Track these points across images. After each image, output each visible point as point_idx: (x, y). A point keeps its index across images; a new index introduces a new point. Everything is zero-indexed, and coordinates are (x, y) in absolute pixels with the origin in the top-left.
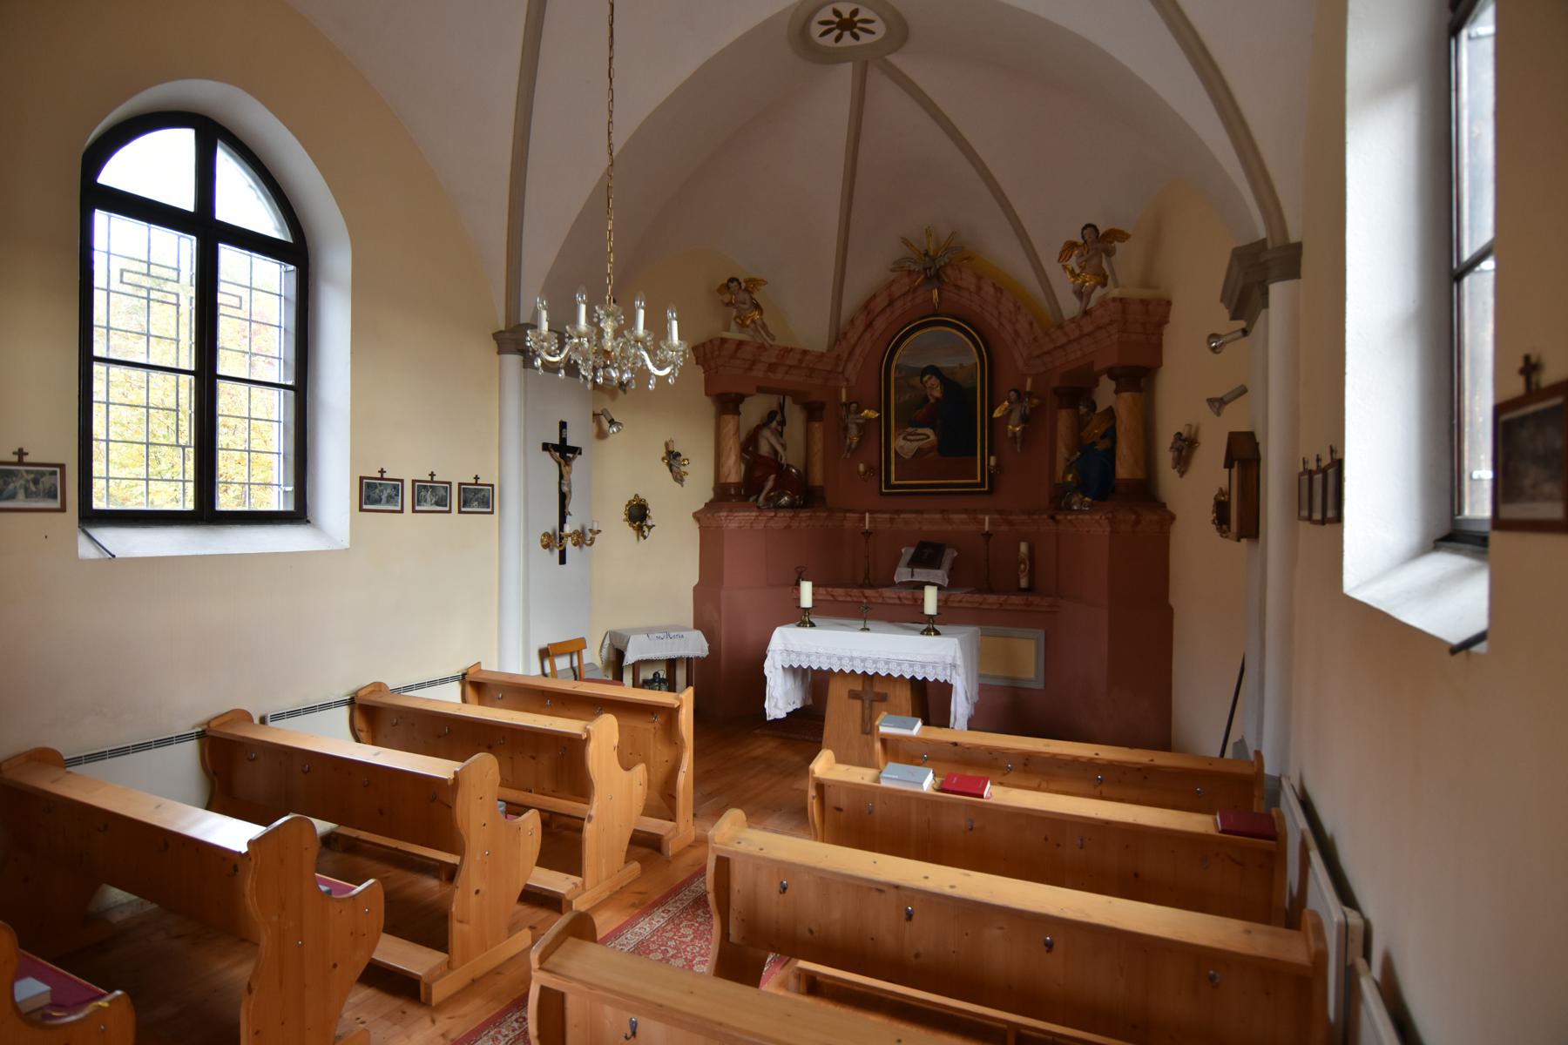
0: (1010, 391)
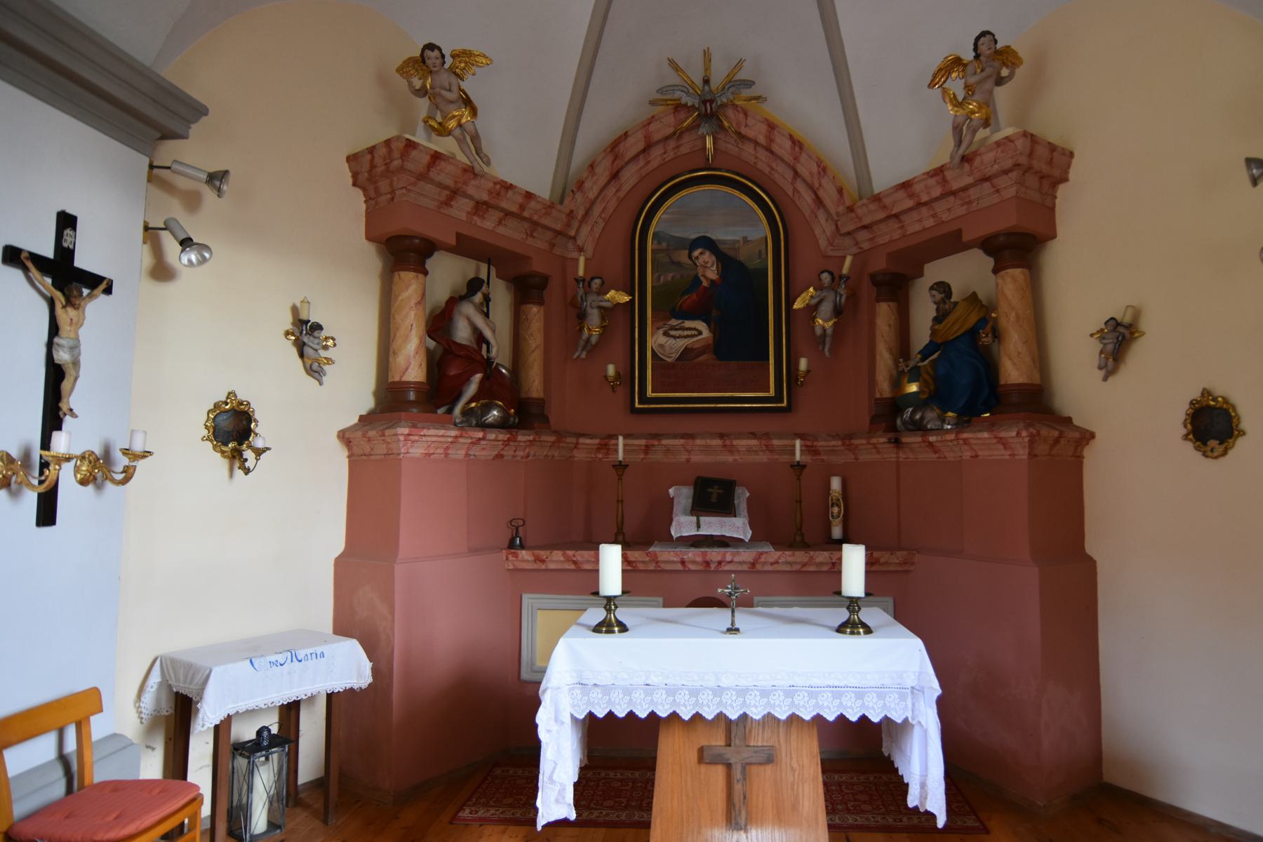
0: (822, 272)
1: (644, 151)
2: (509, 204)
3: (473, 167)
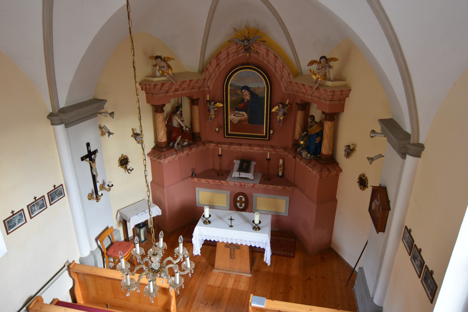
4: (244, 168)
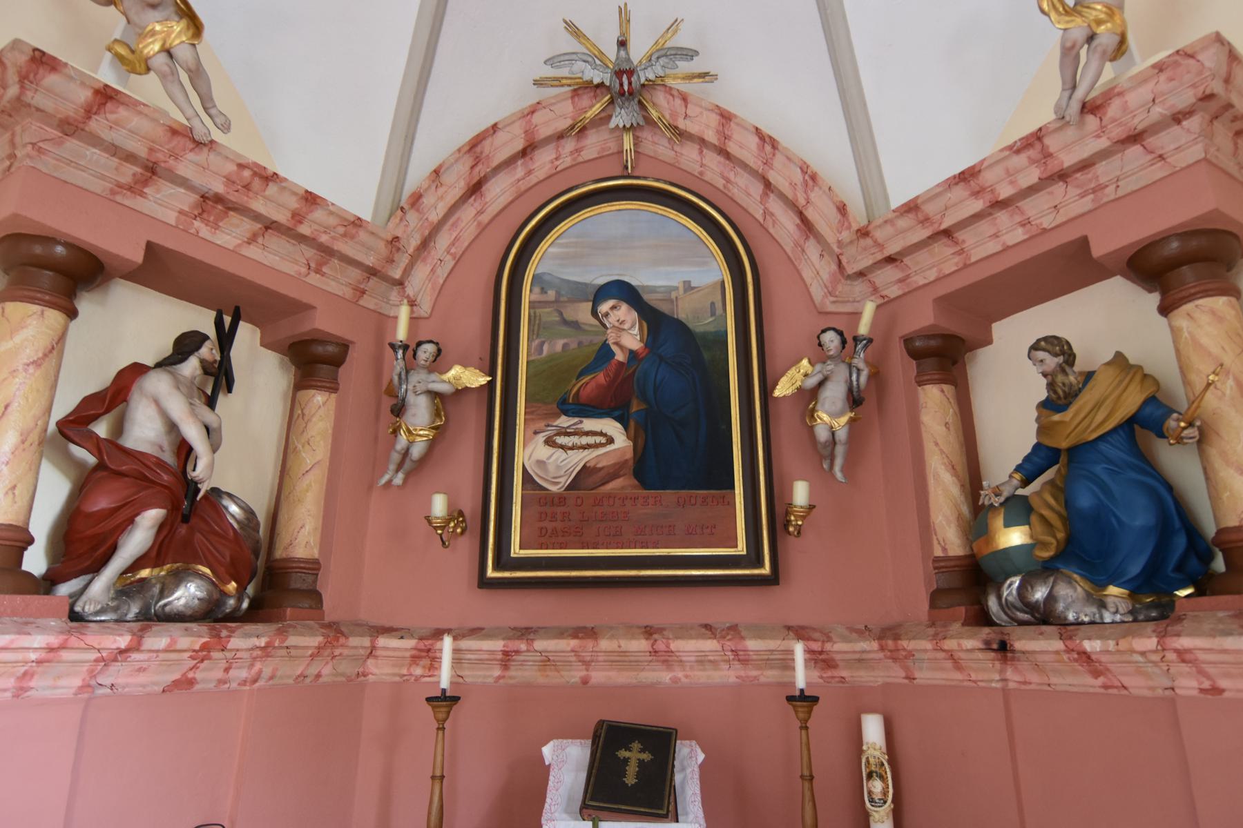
0: (824, 331)
1: (524, 153)
2: (266, 205)
3: (191, 129)
4: (630, 780)
